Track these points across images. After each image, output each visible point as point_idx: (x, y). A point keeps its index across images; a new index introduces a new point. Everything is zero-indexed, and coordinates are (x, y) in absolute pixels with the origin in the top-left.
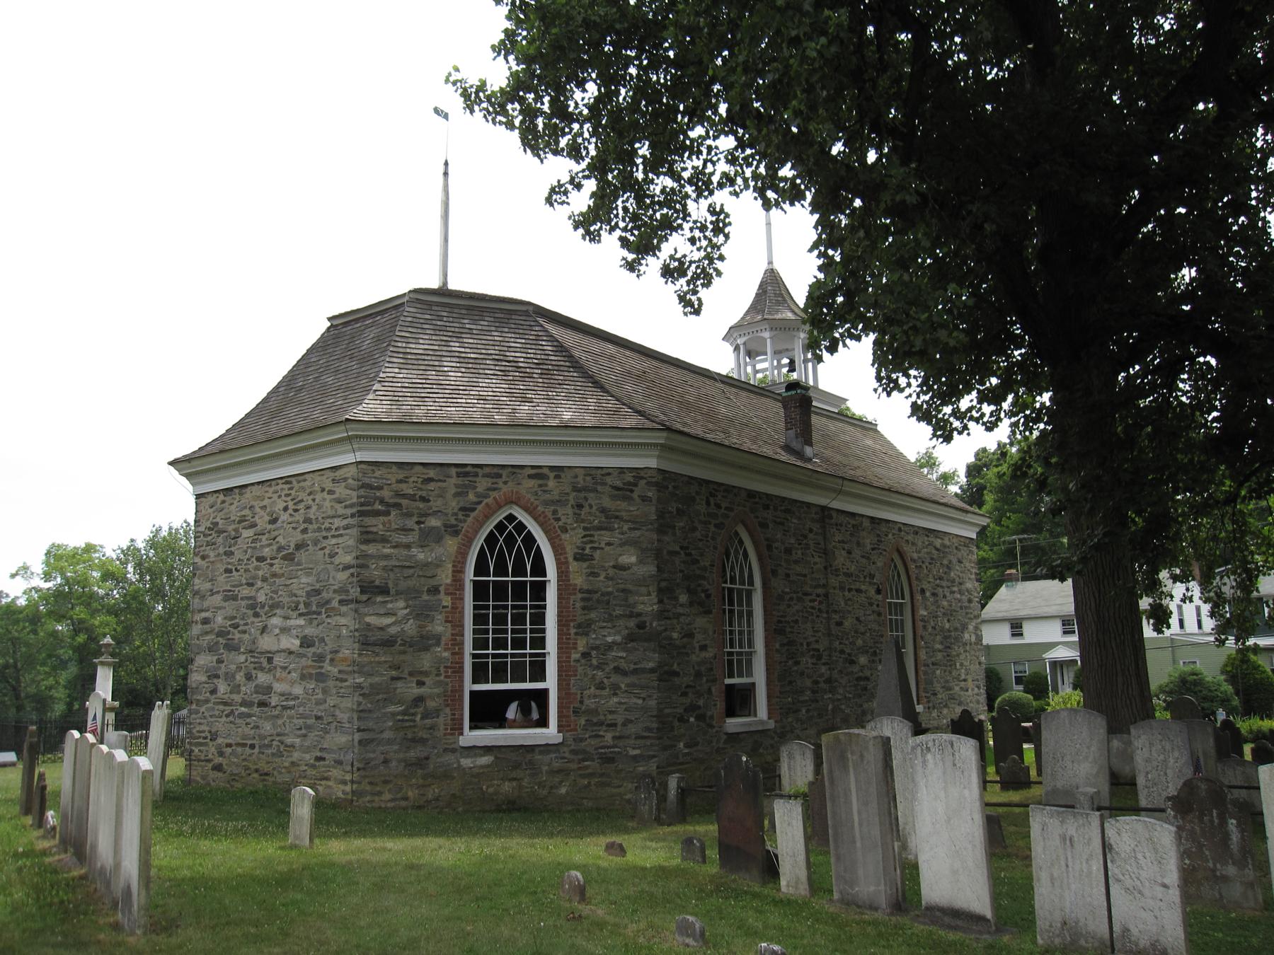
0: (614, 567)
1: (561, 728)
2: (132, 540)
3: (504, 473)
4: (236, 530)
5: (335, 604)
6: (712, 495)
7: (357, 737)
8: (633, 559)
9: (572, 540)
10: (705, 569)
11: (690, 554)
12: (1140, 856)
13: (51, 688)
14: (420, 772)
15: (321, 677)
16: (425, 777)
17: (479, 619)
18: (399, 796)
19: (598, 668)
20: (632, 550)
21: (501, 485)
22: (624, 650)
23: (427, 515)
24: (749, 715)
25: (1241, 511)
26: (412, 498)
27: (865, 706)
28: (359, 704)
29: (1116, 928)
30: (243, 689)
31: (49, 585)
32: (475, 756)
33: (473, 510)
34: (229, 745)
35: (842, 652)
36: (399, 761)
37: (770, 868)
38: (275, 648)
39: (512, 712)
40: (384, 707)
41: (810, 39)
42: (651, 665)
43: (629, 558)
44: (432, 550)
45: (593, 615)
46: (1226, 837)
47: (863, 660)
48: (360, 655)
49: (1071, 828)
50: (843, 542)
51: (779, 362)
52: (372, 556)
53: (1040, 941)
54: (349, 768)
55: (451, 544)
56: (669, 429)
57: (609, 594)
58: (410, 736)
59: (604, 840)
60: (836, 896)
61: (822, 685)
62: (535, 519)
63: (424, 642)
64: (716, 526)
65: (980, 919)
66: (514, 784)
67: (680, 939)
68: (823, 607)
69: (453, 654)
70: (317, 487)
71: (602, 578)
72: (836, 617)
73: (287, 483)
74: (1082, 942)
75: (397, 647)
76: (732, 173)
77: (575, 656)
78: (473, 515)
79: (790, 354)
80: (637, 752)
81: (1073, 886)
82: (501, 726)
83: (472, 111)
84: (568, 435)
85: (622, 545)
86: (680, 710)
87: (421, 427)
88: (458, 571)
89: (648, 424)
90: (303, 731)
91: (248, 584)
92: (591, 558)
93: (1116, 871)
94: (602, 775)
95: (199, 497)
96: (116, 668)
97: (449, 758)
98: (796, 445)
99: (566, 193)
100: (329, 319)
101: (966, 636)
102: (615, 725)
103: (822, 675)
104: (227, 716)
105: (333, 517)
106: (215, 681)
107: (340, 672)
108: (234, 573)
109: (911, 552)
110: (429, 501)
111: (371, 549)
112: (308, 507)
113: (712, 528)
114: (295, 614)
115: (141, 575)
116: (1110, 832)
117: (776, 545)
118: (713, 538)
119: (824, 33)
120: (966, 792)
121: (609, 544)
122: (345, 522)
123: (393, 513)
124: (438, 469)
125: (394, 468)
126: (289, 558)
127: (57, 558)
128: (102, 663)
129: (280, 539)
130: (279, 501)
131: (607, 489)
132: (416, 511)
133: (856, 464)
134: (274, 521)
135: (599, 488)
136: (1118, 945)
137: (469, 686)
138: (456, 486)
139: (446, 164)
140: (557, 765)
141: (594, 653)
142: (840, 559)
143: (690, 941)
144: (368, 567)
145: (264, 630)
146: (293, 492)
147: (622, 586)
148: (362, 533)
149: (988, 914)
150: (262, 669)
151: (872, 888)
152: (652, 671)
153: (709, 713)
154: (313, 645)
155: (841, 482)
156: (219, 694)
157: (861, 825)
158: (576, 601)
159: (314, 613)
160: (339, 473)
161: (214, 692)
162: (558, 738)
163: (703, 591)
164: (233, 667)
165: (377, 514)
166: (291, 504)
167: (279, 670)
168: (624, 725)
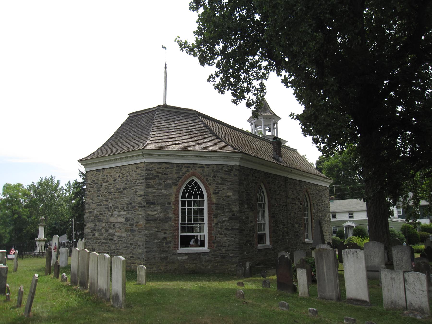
0: (225, 196)
2: (33, 183)
3: (191, 166)
4: (101, 183)
5: (137, 207)
6: (254, 173)
7: (145, 250)
8: (231, 194)
9: (212, 188)
12: (415, 283)
13: (4, 233)
14: (165, 261)
15: (132, 231)
17: (183, 213)
18: (158, 269)
19: (220, 228)
21: (190, 170)
23: (167, 179)
24: (263, 243)
25: (415, 180)
26: (162, 174)
27: (297, 241)
28: (146, 239)
29: (408, 303)
30: (104, 234)
31: (5, 197)
32: (182, 256)
33: (181, 178)
35: (291, 223)
36: (158, 258)
37: (295, 289)
38: (116, 221)
39: (192, 242)
41: (310, 42)
42: (236, 227)
43: (230, 194)
44: (169, 190)
45: (219, 212)
48: (146, 224)
49: (394, 275)
52: (150, 192)
53: (384, 307)
54: (142, 260)
55: (174, 188)
56: (243, 153)
57: (224, 205)
58: (162, 250)
59: (236, 282)
60: (319, 296)
61: (285, 234)
62: (201, 181)
63: (166, 220)
64: (255, 183)
65: (365, 302)
66: (194, 265)
67: (281, 308)
69: (175, 224)
70: (130, 170)
71: (221, 200)
72: (289, 212)
73: (119, 168)
74: (397, 307)
75: (158, 221)
76: (265, 73)
77: (213, 224)
78: (181, 179)
79: (269, 126)
80: (232, 255)
82: (188, 247)
83: (183, 51)
84: (211, 155)
85: (227, 189)
86: (245, 242)
87: (166, 151)
88: (177, 197)
89: (236, 151)
90: (126, 248)
92: (218, 193)
93: (408, 287)
94: (221, 262)
96: (45, 227)
97: (174, 257)
98: (276, 157)
99: (214, 78)
100: (129, 114)
101: (326, 218)
102: (225, 246)
104: (98, 243)
105: (136, 179)
106: (94, 232)
107: (139, 229)
108: (101, 197)
109: (310, 191)
110: (167, 175)
111: (150, 190)
112: (127, 176)
113: (254, 184)
114: (123, 211)
115: (36, 194)
116: (406, 276)
117: (272, 189)
118: (254, 187)
119: (315, 40)
120: (361, 265)
121: (224, 189)
122: (141, 181)
123: (156, 179)
124: (170, 164)
125: (157, 164)
126: (121, 192)
128: (41, 225)
129: (117, 186)
132: (163, 178)
133: (293, 163)
134: (115, 180)
135: (221, 171)
136: (408, 308)
137: (180, 234)
138: (176, 170)
139: (166, 64)
140: (207, 259)
141: (219, 224)
143: (284, 309)
144: (148, 196)
145: (112, 215)
146: (122, 171)
147: (228, 202)
148: (147, 185)
149: (368, 300)
150: (111, 228)
151: (331, 294)
152: (237, 229)
154: (129, 221)
155: (291, 169)
156: (96, 236)
157: (327, 275)
158: (214, 207)
159: (130, 210)
160: (138, 166)
161: (94, 235)
162: (208, 251)
164: (101, 227)
165: (151, 179)
166: (121, 175)
167: (117, 228)
168: (228, 246)
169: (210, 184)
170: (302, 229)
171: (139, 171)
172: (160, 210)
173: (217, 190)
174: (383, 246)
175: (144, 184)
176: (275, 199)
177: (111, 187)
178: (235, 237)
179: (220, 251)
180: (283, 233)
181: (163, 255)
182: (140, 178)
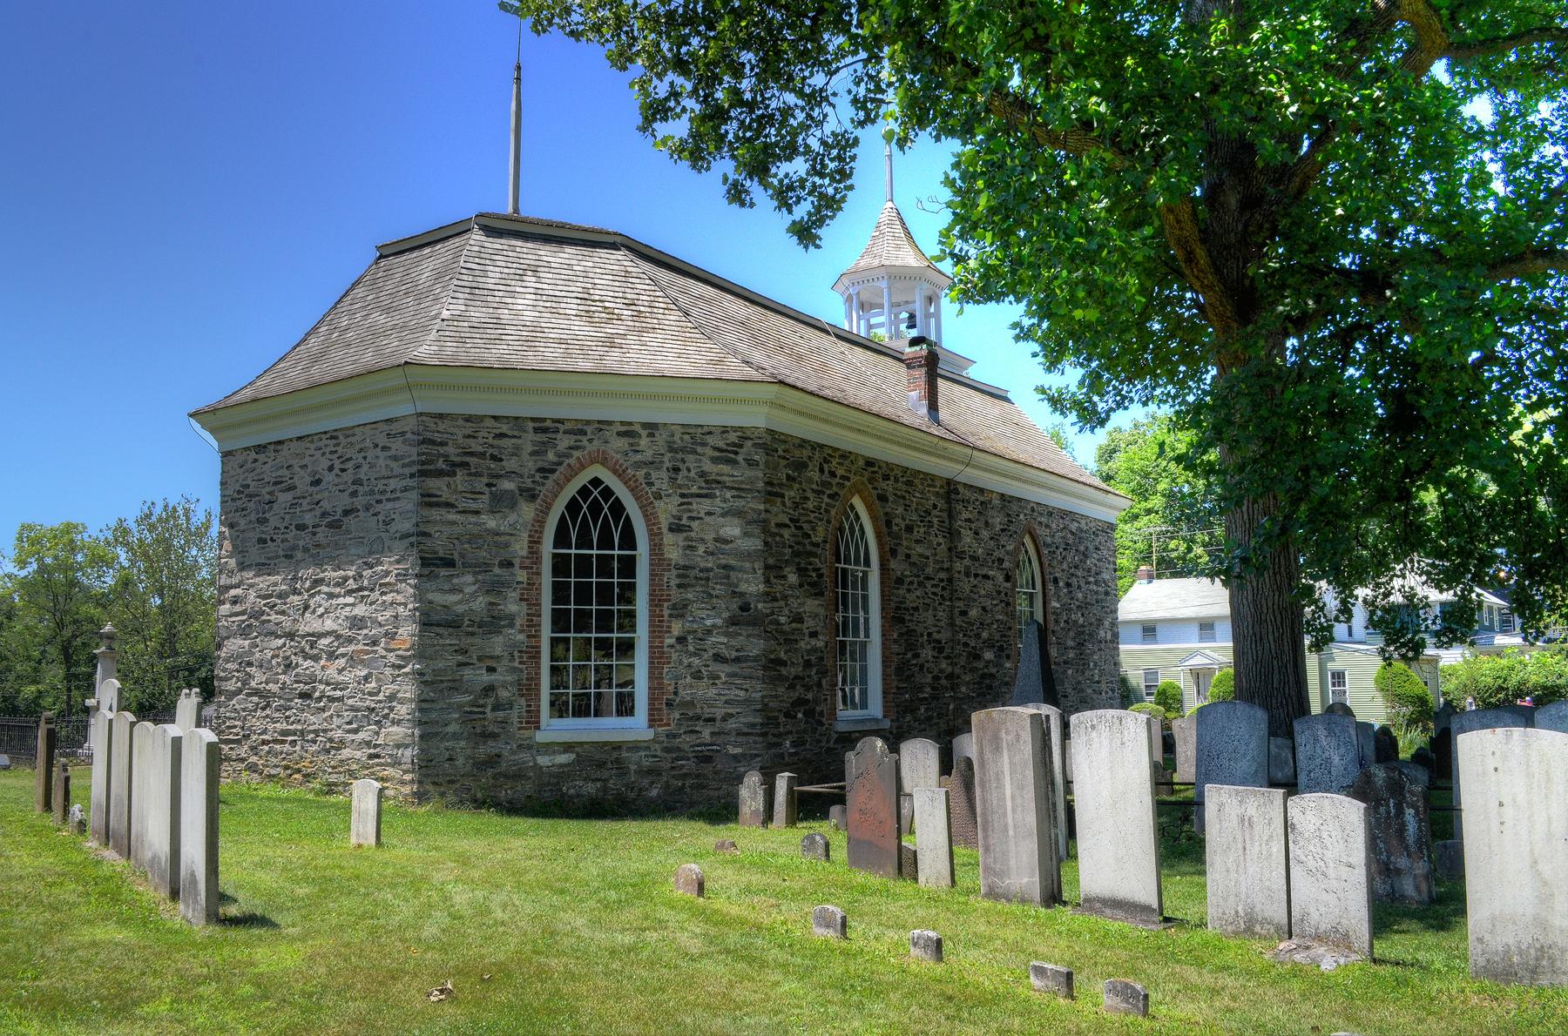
1: (652, 722)
8: (737, 532)
10: (817, 545)
11: (801, 528)
12: (1325, 835)
16: (495, 777)
19: (695, 654)
20: (736, 521)
21: (586, 443)
22: (726, 634)
23: (498, 476)
26: (482, 455)
32: (554, 752)
33: (553, 471)
34: (264, 742)
36: (468, 758)
40: (449, 697)
42: (755, 652)
43: (732, 529)
46: (1402, 830)
47: (989, 655)
50: (969, 520)
51: (896, 316)
55: (527, 511)
57: (708, 570)
61: (944, 682)
64: (830, 496)
66: (599, 785)
68: (946, 594)
70: (368, 443)
73: (332, 438)
80: (738, 751)
81: (1250, 871)
85: (723, 515)
88: (535, 542)
91: (286, 556)
93: (1299, 852)
95: (226, 455)
97: (524, 756)
100: (378, 248)
101: (1102, 633)
102: (713, 720)
103: (941, 671)
111: (435, 514)
113: (826, 500)
116: (1294, 812)
121: (709, 514)
127: (30, 540)
130: (323, 460)
131: (709, 452)
135: (699, 449)
139: (519, 68)
140: (646, 763)
141: (690, 638)
142: (967, 538)
146: (339, 449)
152: (756, 659)
153: (818, 709)
157: (1014, 811)
162: (648, 735)
163: (815, 570)
165: (440, 473)
169: (658, 496)
170: (1008, 665)
171: (397, 446)
172: (474, 588)
173: (685, 516)
174: (1266, 717)
175: (414, 496)
176: (908, 556)
177: (305, 507)
178: (747, 684)
179: (694, 736)
180: (936, 678)
181: (484, 751)
182: (401, 471)
